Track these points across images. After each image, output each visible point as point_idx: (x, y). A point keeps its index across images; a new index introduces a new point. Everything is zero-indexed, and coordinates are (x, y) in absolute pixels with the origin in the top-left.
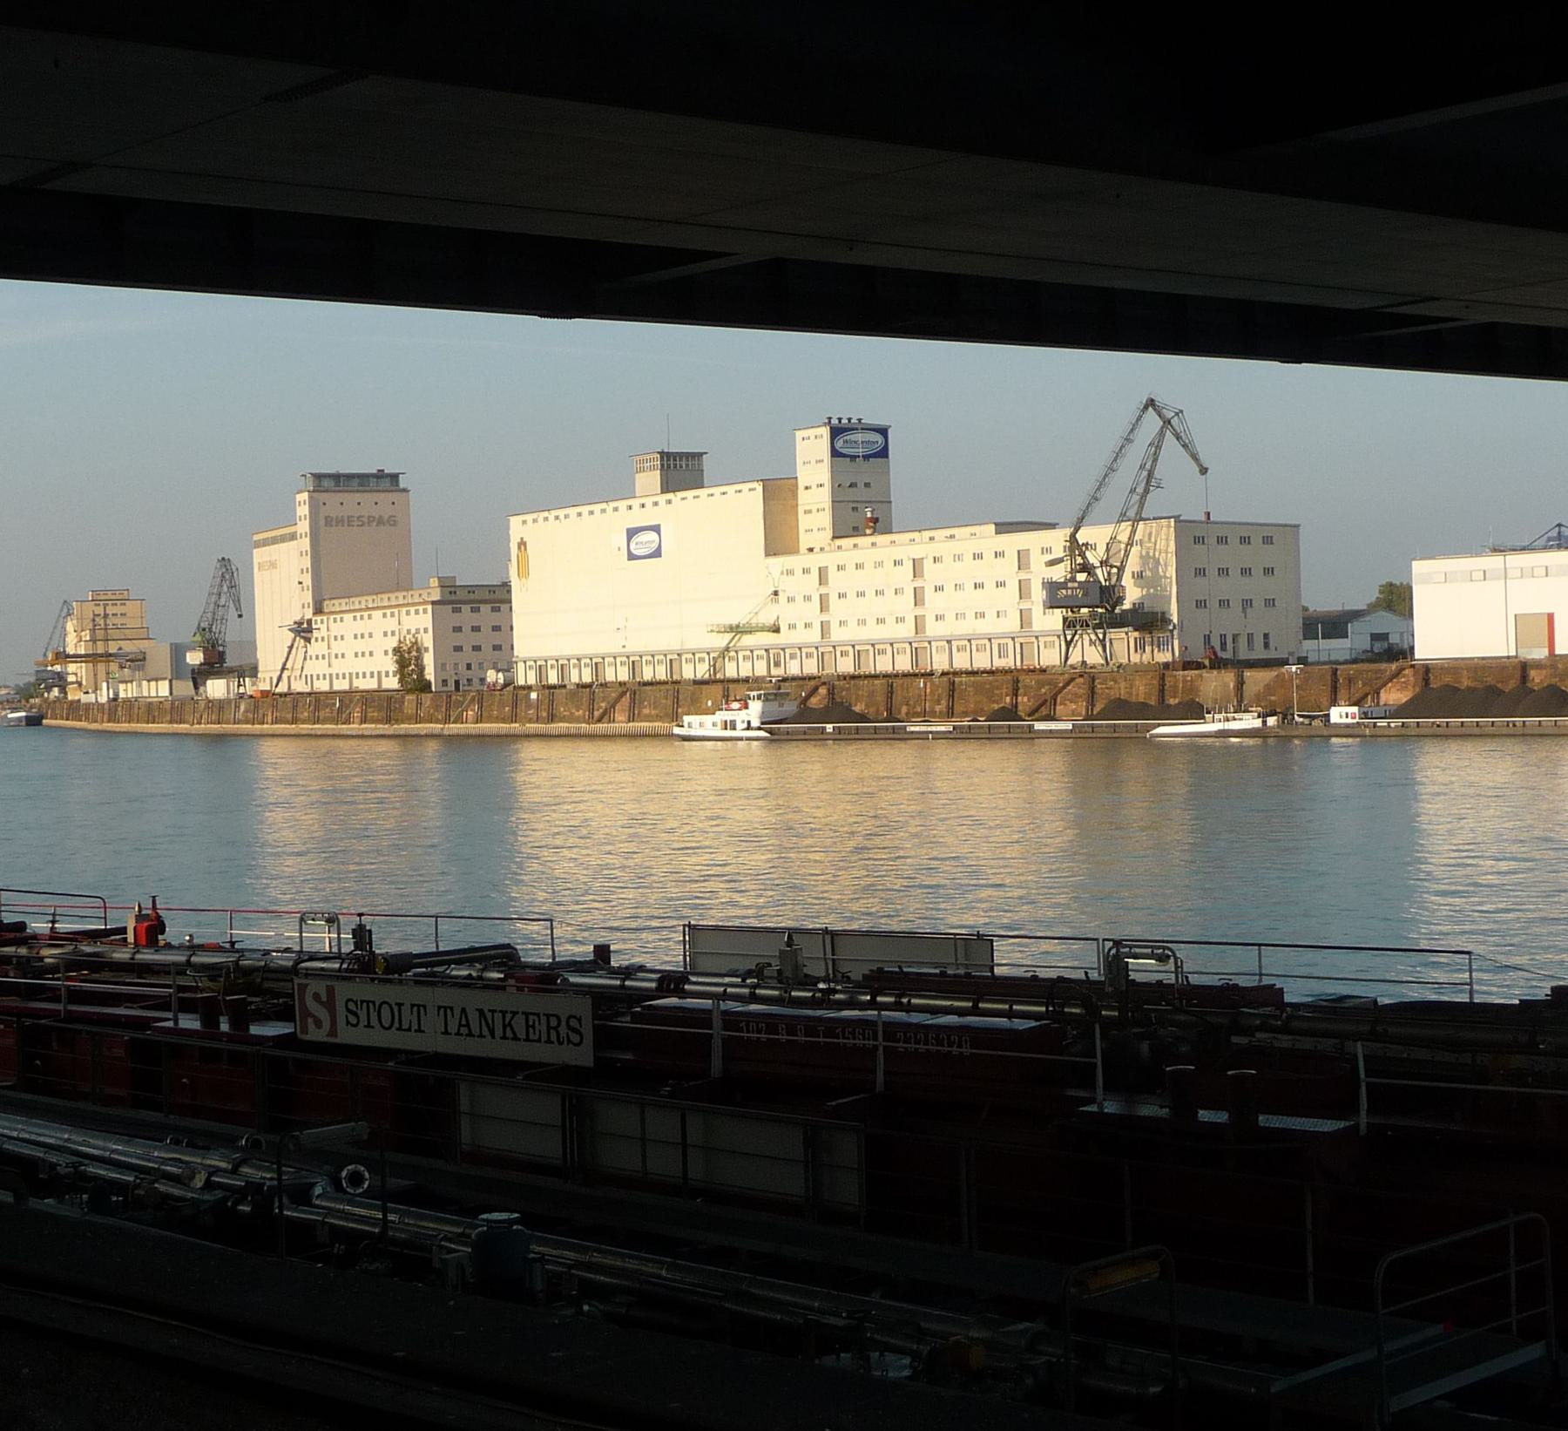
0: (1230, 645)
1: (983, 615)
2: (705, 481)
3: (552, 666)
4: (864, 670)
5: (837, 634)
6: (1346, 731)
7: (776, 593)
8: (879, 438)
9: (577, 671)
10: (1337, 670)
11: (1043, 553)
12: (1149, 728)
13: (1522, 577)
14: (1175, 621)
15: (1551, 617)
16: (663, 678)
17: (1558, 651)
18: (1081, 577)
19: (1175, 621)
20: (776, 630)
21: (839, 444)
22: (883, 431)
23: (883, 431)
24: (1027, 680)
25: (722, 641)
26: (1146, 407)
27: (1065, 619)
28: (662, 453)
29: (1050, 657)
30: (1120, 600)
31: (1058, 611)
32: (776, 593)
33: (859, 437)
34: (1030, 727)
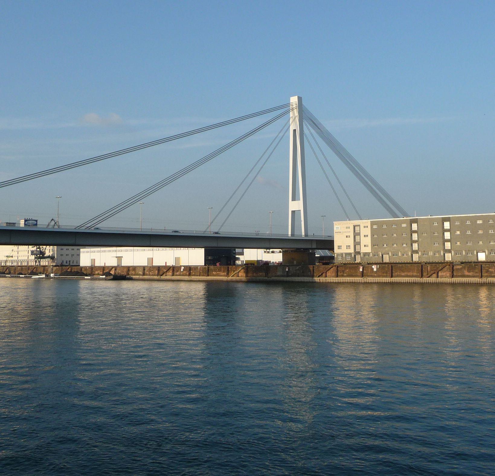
0: (68, 263)
1: (66, 255)
2: (296, 198)
3: (47, 261)
4: (22, 265)
5: (20, 258)
6: (52, 278)
7: (13, 250)
8: (35, 222)
9: (45, 263)
10: (229, 267)
11: (349, 227)
12: (31, 277)
13: (131, 251)
14: (56, 258)
15: (95, 259)
16: (4, 265)
17: (106, 265)
18: (38, 250)
19: (56, 258)
20: (12, 257)
21: (26, 223)
22: (36, 221)
23: (36, 221)
24: (30, 268)
25: (5, 259)
26: (52, 220)
27: (35, 257)
28: (7, 223)
29: (33, 264)
30: (45, 254)
31: (34, 256)
32: (13, 250)
33: (31, 222)
34: (84, 278)
